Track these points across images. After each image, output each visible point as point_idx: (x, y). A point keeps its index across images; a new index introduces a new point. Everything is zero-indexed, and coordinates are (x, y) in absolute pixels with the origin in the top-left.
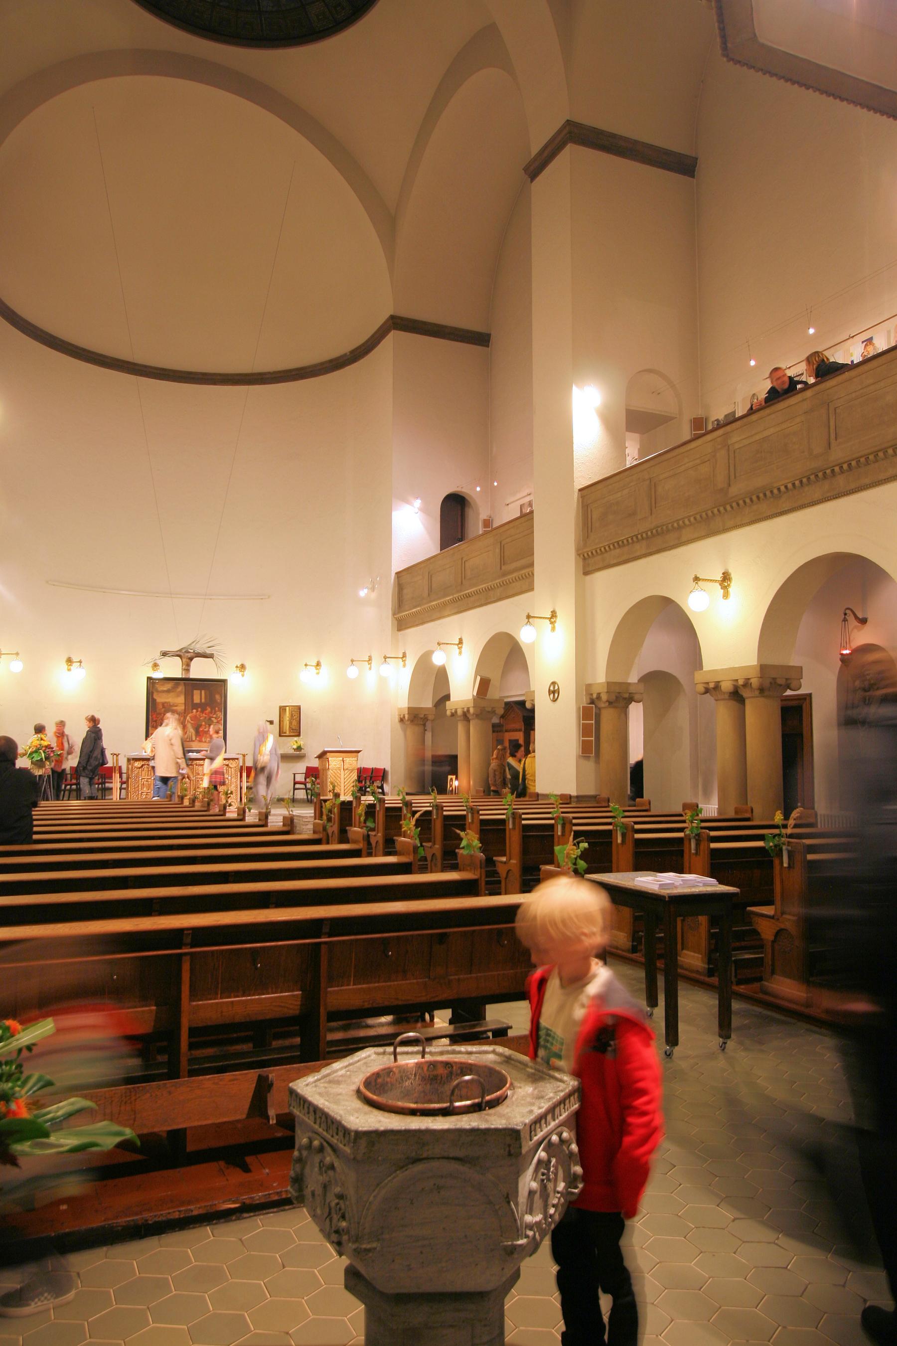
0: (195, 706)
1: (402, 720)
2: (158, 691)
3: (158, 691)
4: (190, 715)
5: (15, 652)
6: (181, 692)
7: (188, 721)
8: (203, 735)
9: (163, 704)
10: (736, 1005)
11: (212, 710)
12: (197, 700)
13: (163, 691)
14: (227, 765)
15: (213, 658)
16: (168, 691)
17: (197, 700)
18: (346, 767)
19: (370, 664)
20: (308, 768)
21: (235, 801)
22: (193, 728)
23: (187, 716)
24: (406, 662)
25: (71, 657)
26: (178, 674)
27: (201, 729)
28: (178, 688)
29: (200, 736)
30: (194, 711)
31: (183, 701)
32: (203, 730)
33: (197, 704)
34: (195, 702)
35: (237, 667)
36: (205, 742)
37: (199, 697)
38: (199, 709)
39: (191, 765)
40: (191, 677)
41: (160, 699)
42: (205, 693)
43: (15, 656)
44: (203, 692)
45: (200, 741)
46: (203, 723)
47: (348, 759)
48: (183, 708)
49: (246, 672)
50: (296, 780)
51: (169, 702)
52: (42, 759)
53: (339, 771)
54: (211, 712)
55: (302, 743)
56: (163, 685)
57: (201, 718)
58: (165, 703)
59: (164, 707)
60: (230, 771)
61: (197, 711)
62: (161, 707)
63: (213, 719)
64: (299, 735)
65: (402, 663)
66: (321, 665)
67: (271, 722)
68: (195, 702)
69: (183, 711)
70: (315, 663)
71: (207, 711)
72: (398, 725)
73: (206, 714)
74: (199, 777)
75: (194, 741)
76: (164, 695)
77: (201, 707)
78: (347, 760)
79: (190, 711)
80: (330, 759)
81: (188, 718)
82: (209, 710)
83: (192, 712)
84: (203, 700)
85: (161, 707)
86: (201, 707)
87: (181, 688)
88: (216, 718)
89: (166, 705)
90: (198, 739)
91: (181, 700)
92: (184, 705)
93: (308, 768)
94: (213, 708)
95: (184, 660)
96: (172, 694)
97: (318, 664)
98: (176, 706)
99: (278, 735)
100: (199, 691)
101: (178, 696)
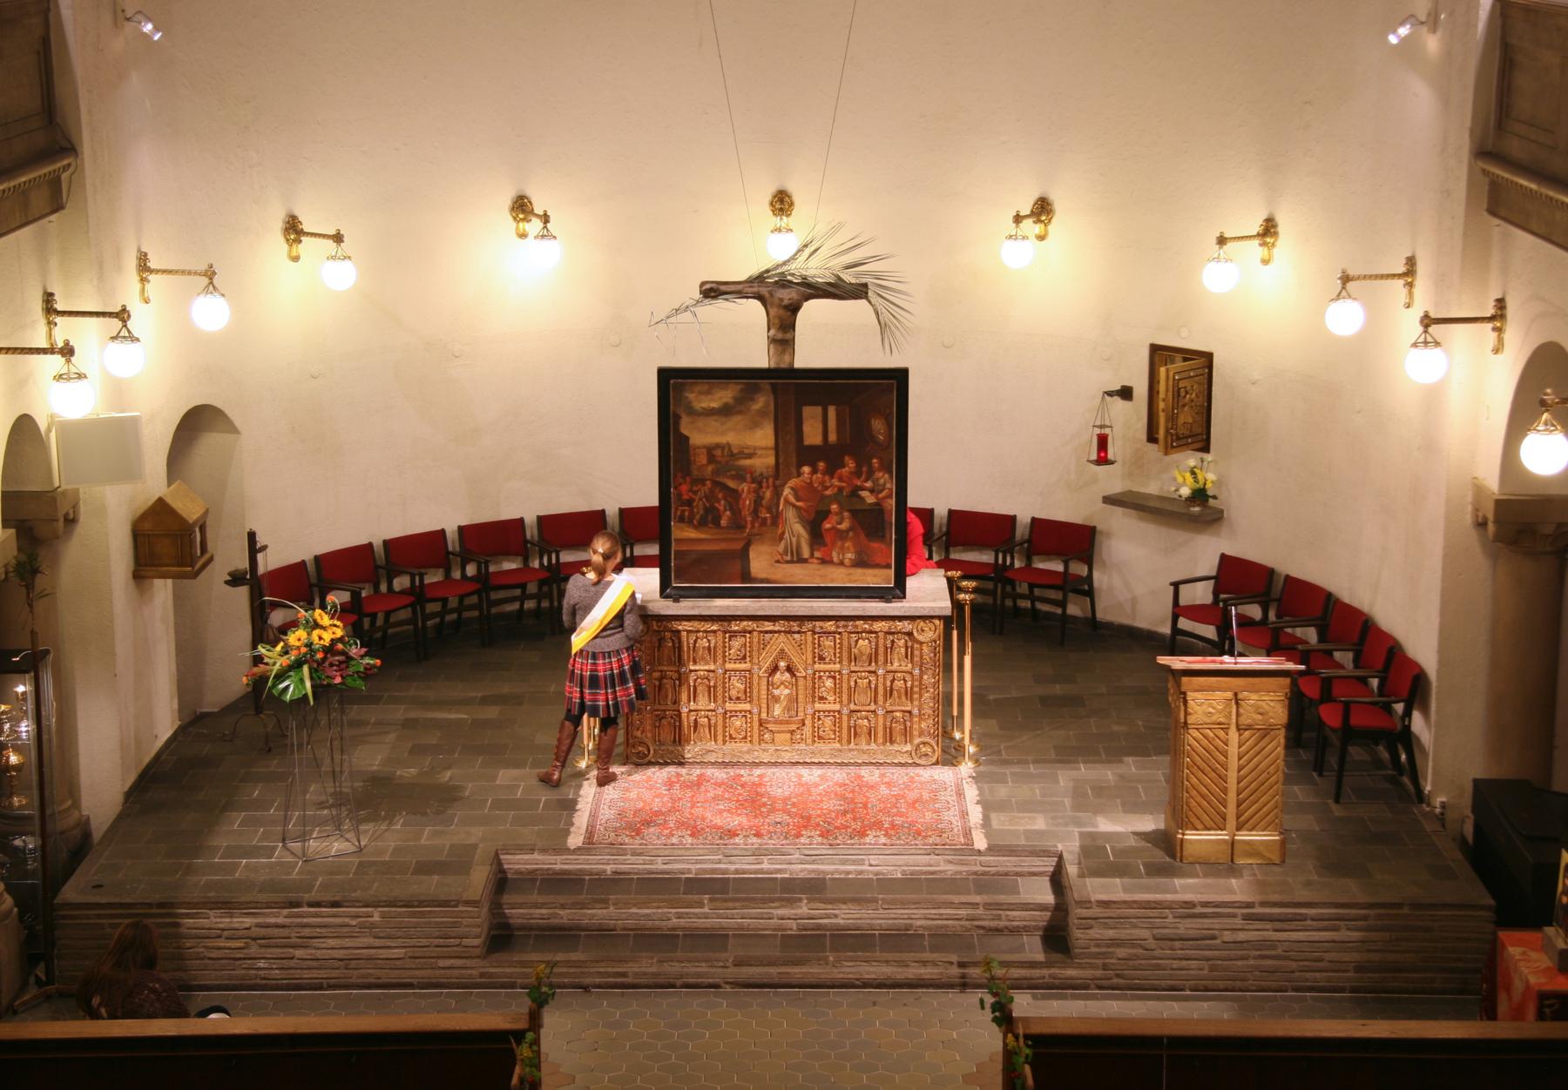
0: (808, 455)
1: (1481, 524)
2: (692, 412)
3: (692, 412)
4: (792, 483)
5: (333, 232)
6: (762, 414)
7: (787, 501)
8: (834, 544)
9: (710, 450)
10: (410, 609)
11: (859, 466)
12: (812, 435)
13: (711, 413)
14: (910, 634)
15: (866, 297)
16: (725, 411)
17: (812, 435)
18: (1244, 721)
19: (1410, 285)
20: (1225, 560)
21: (933, 743)
22: (802, 520)
23: (784, 485)
24: (1507, 336)
25: (529, 193)
26: (757, 355)
27: (827, 526)
28: (753, 400)
29: (826, 545)
30: (806, 469)
31: (770, 441)
32: (833, 528)
33: (812, 448)
34: (807, 442)
35: (1018, 219)
36: (841, 563)
37: (819, 427)
38: (821, 465)
39: (799, 632)
40: (798, 364)
41: (701, 435)
42: (838, 415)
43: (330, 243)
44: (832, 411)
45: (825, 561)
46: (834, 507)
47: (1254, 697)
48: (771, 460)
49: (1057, 226)
50: (1182, 602)
51: (728, 444)
52: (306, 695)
53: (1221, 734)
54: (858, 474)
55: (1211, 477)
56: (708, 393)
57: (828, 492)
58: (718, 446)
59: (711, 458)
60: (917, 653)
61: (814, 471)
62: (702, 459)
63: (864, 494)
64: (1206, 448)
65: (1492, 337)
66: (1276, 234)
67: (1126, 393)
68: (807, 442)
69: (771, 472)
70: (1255, 227)
71: (845, 471)
72: (1472, 537)
73: (841, 479)
74: (823, 667)
75: (805, 561)
76: (713, 423)
77: (828, 456)
78: (1251, 699)
79: (794, 470)
80: (1190, 695)
81: (787, 491)
82: (851, 464)
83: (799, 474)
84: (833, 437)
85: (705, 461)
86: (828, 456)
87: (762, 401)
88: (872, 491)
89: (718, 452)
90: (817, 554)
91: (763, 437)
92: (773, 452)
93: (1225, 560)
94: (863, 461)
95: (773, 311)
96: (737, 419)
97: (1269, 229)
98: (750, 456)
99: (1144, 437)
100: (819, 409)
101: (755, 425)
